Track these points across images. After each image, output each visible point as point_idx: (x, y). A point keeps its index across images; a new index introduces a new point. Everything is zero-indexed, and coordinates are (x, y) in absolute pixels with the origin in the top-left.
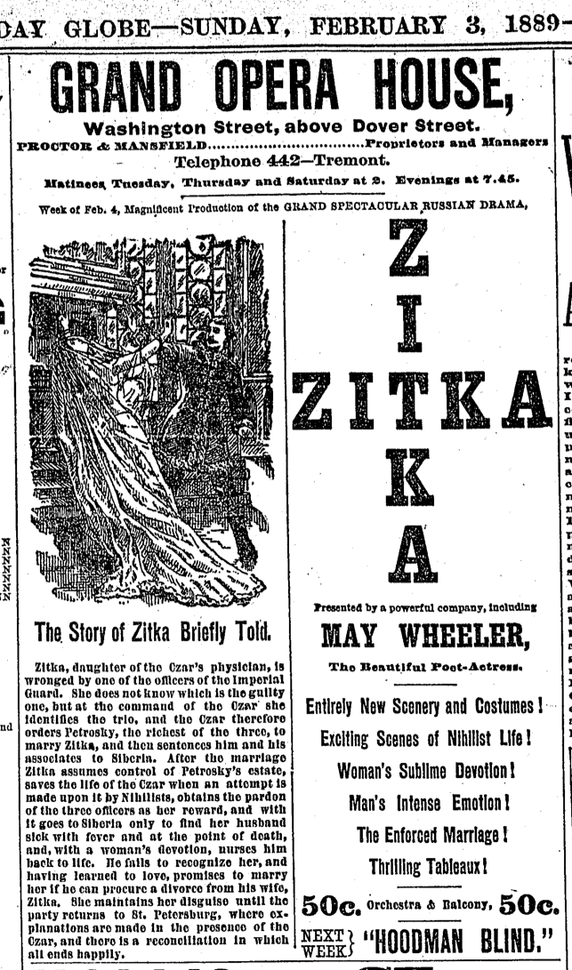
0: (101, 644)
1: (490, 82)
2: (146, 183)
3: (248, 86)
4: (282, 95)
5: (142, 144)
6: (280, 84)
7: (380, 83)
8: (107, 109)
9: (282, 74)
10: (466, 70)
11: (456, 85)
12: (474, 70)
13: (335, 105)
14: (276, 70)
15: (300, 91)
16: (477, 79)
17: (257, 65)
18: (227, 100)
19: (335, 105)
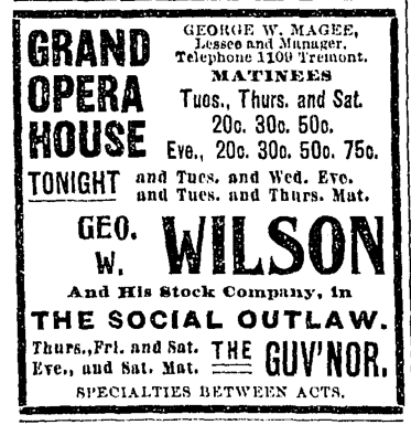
2: (276, 296)
5: (279, 73)
6: (90, 94)
9: (93, 86)
12: (121, 131)
17: (68, 79)
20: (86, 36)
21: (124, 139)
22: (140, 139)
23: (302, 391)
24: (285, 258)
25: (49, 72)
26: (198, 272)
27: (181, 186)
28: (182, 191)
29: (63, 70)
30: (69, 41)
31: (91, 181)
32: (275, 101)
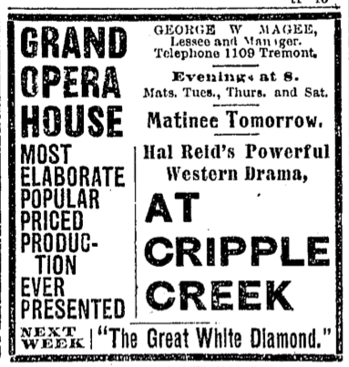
9: (77, 76)
17: (56, 70)
20: (71, 34)
21: (104, 121)
22: (118, 121)
25: (38, 62)
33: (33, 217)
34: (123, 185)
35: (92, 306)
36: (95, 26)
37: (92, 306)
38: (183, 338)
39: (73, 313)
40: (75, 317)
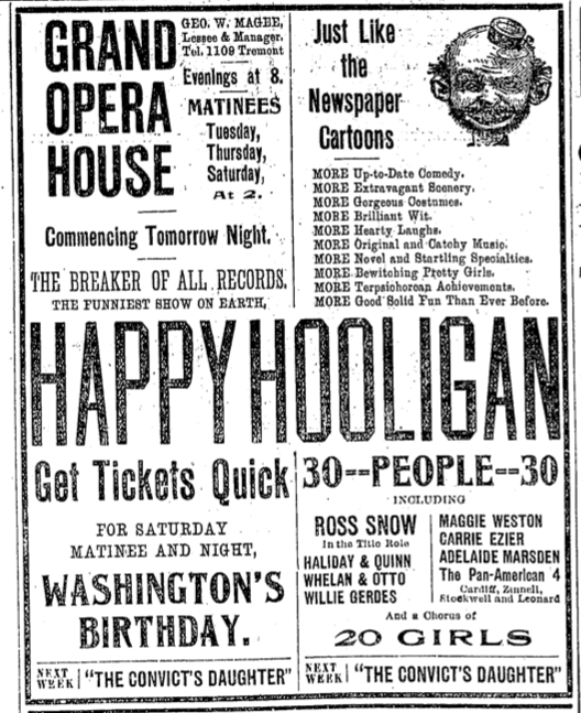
0: (466, 194)
1: (161, 170)
3: (80, 109)
4: (114, 119)
6: (112, 108)
7: (53, 169)
8: (102, 68)
9: (114, 97)
10: (137, 157)
11: (126, 172)
12: (145, 157)
13: (167, 128)
14: (108, 93)
15: (132, 115)
16: (148, 167)
17: (89, 88)
18: (58, 123)
19: (167, 128)
23: (390, 614)
24: (101, 597)
26: (105, 22)
27: (211, 142)
28: (210, 146)
29: (84, 76)
30: (90, 37)
31: (516, 674)
32: (235, 154)
33: (78, 98)
34: (122, 686)
35: (527, 671)
36: (137, 18)
37: (527, 671)
38: (255, 76)
39: (541, 678)
40: (543, 681)
